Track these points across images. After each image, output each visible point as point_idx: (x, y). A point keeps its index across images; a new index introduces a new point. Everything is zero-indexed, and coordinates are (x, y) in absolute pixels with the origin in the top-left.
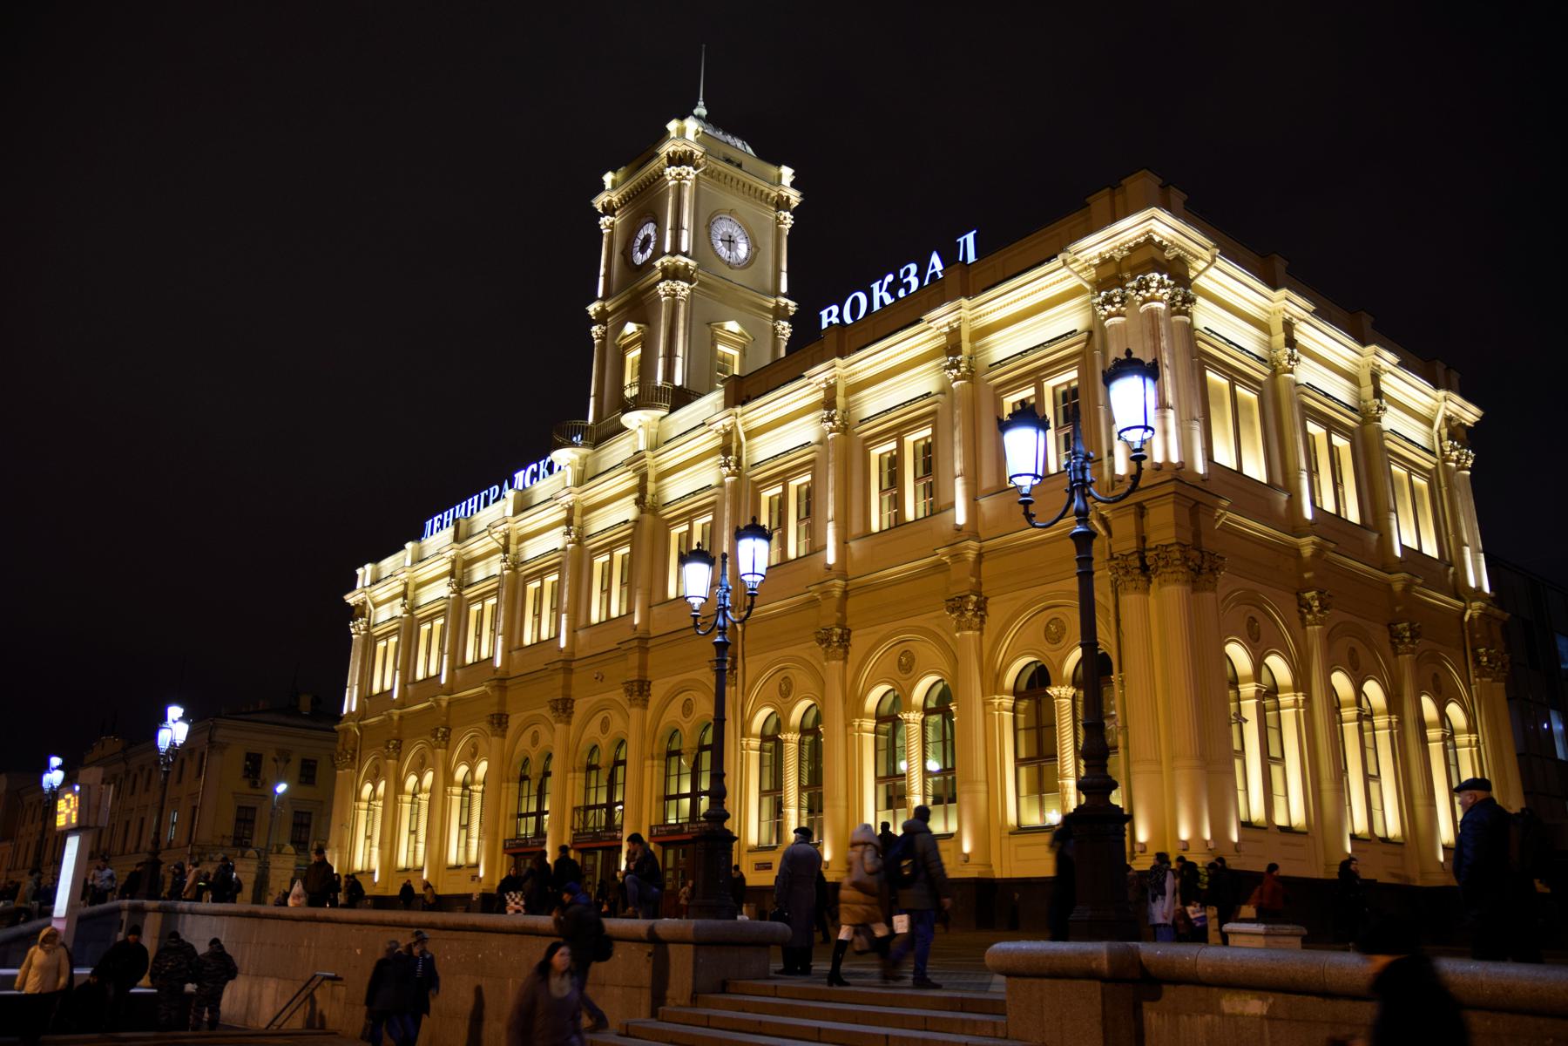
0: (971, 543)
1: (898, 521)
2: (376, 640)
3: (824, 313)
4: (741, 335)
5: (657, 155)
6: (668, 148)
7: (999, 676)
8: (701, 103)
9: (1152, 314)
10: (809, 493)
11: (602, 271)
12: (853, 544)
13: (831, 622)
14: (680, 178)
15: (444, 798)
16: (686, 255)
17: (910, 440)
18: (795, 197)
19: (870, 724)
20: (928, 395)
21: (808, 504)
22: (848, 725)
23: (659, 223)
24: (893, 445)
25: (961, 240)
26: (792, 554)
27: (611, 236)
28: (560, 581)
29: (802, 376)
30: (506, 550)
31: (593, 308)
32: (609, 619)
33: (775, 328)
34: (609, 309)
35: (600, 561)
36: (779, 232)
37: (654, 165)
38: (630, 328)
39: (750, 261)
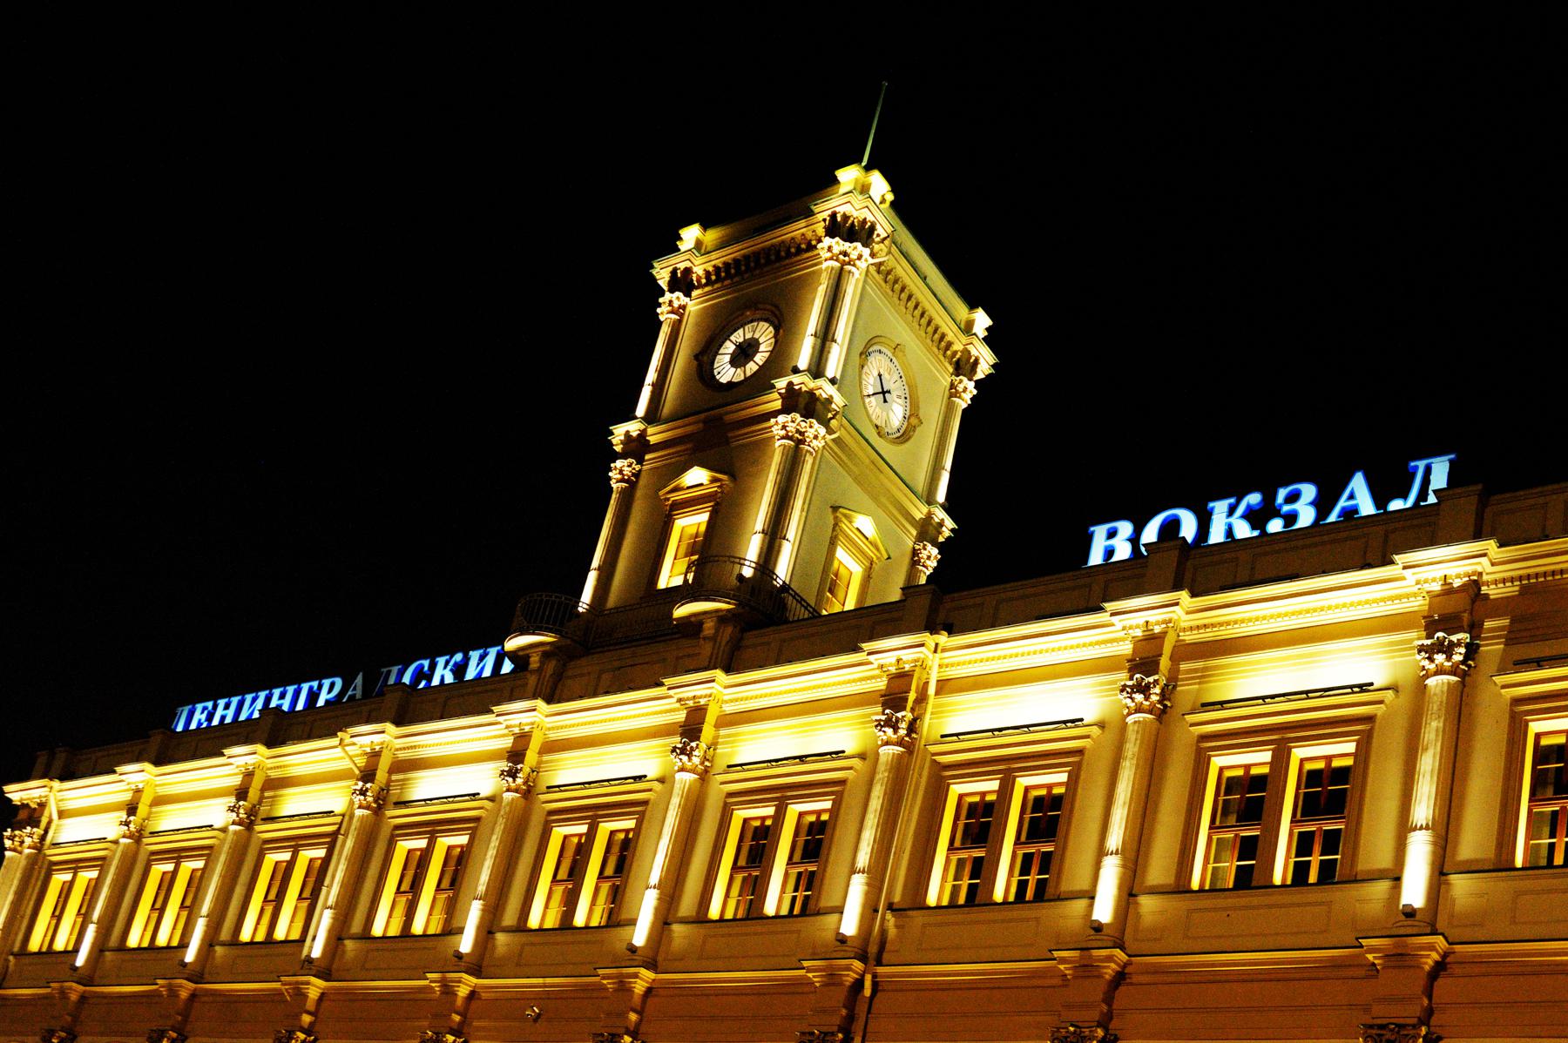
0: (643, 972)
1: (977, 897)
2: (51, 868)
3: (1100, 532)
5: (811, 213)
6: (823, 210)
10: (626, 844)
11: (651, 376)
12: (677, 929)
14: (845, 261)
17: (605, 828)
18: (986, 361)
20: (1363, 688)
21: (456, 872)
23: (784, 324)
24: (992, 785)
25: (1421, 464)
26: (579, 920)
27: (676, 328)
28: (98, 883)
29: (857, 650)
30: (132, 809)
32: (269, 940)
33: (915, 553)
34: (653, 440)
35: (158, 869)
36: (950, 407)
37: (797, 230)
38: (697, 476)
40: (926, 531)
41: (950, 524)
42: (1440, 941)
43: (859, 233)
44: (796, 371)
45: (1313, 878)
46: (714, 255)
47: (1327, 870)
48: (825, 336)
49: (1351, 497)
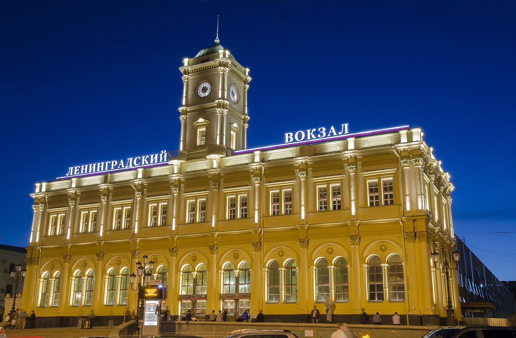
1: (193, 222)
4: (237, 128)
7: (364, 259)
8: (217, 38)
9: (419, 168)
11: (184, 95)
13: (304, 237)
14: (224, 71)
15: (261, 273)
16: (226, 99)
18: (249, 79)
19: (181, 274)
22: (69, 278)
27: (187, 82)
31: (180, 109)
33: (243, 126)
36: (244, 91)
38: (201, 120)
39: (237, 102)
40: (244, 120)
41: (249, 118)
42: (359, 221)
43: (225, 65)
44: (219, 99)
45: (374, 205)
46: (193, 66)
47: (392, 202)
48: (223, 90)
49: (332, 131)
